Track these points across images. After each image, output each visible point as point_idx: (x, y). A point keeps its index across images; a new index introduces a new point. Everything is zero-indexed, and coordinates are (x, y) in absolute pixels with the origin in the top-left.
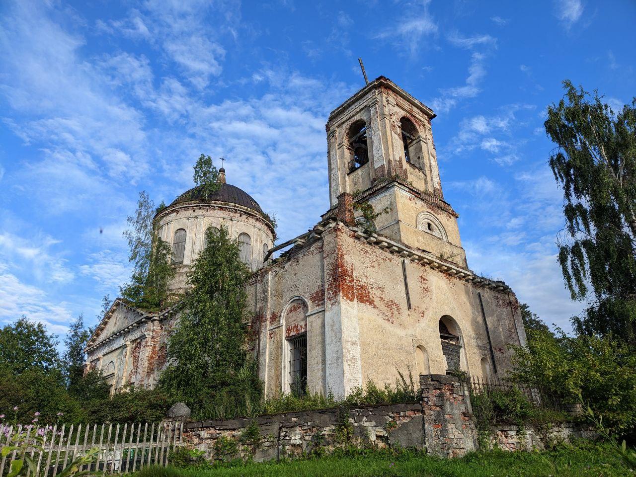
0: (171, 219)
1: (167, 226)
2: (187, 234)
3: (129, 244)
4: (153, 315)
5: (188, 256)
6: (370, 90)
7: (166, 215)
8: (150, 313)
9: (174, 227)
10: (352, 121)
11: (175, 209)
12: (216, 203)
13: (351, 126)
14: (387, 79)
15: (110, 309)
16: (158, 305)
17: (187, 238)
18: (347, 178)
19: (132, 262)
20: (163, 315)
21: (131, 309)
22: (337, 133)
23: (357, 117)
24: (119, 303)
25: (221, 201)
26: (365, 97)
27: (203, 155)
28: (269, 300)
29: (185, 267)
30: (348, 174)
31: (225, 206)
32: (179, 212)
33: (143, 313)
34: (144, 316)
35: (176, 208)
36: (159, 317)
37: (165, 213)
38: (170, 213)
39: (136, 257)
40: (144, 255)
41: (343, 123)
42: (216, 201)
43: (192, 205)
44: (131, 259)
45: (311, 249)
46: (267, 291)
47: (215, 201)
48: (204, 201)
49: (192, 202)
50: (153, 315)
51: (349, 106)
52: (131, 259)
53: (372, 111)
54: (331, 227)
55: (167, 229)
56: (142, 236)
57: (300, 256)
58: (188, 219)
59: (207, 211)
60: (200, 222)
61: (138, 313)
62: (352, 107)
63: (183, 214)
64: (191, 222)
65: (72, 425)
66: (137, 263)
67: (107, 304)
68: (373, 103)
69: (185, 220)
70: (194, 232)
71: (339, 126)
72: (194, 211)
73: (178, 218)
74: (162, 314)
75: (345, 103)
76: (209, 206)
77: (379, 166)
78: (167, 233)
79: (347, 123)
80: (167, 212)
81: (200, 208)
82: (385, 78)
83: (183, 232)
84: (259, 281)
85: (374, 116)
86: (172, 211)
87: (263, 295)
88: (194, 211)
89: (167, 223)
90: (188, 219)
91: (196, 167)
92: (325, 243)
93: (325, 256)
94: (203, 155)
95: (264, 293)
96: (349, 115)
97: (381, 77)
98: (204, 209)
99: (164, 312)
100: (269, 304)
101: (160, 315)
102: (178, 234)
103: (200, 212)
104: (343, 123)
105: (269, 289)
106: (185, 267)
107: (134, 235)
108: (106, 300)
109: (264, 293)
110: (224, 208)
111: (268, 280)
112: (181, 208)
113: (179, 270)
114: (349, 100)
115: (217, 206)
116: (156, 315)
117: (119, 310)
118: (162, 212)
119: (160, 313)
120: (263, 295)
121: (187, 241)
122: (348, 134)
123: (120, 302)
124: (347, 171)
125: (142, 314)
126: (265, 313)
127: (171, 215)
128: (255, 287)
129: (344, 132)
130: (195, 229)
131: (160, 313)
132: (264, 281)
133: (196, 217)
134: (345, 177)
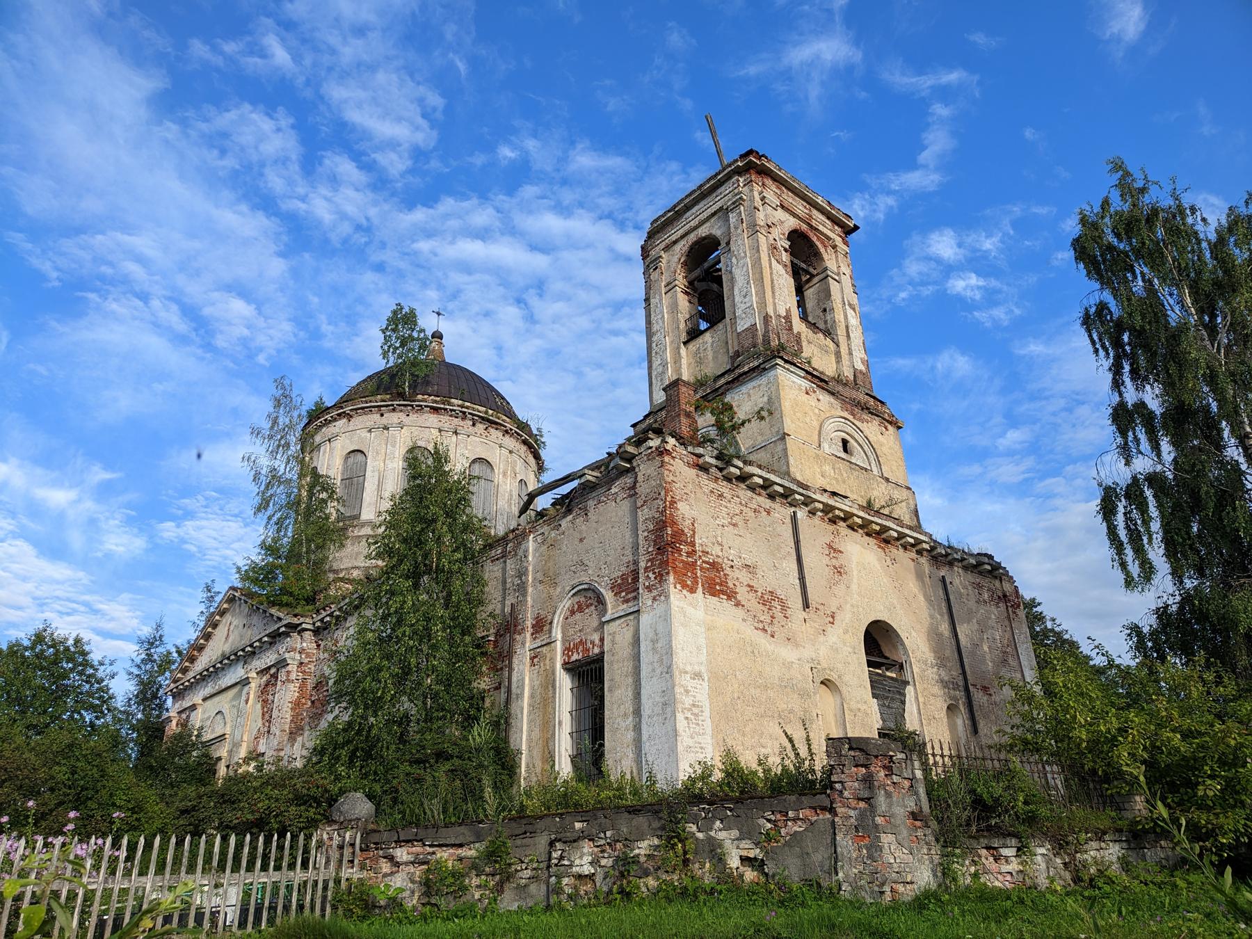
3: (254, 480)
6: (728, 177)
7: (327, 423)
8: (295, 616)
9: (342, 447)
10: (692, 237)
12: (424, 400)
13: (692, 248)
14: (763, 156)
16: (311, 600)
17: (369, 468)
18: (683, 351)
19: (260, 515)
20: (322, 620)
21: (258, 608)
22: (664, 261)
23: (703, 231)
26: (719, 191)
28: (530, 590)
30: (685, 343)
33: (281, 615)
34: (284, 622)
35: (347, 409)
36: (314, 624)
37: (326, 420)
38: (335, 420)
39: (268, 505)
41: (675, 242)
45: (613, 490)
46: (525, 573)
48: (401, 396)
50: (302, 620)
51: (688, 208)
53: (733, 217)
54: (651, 448)
56: (280, 465)
57: (591, 503)
58: (370, 431)
61: (272, 615)
62: (694, 210)
63: (360, 421)
66: (269, 518)
67: (211, 599)
68: (733, 203)
69: (365, 434)
71: (667, 249)
72: (382, 415)
73: (350, 429)
74: (319, 618)
75: (678, 203)
77: (746, 327)
79: (682, 243)
80: (328, 417)
81: (394, 410)
82: (757, 153)
83: (359, 457)
85: (736, 228)
86: (339, 415)
87: (517, 581)
88: (382, 415)
90: (370, 431)
91: (387, 328)
92: (640, 478)
93: (639, 504)
95: (520, 577)
96: (687, 227)
97: (750, 152)
99: (324, 614)
100: (529, 599)
101: (315, 620)
102: (351, 460)
103: (392, 418)
104: (675, 242)
105: (530, 568)
107: (265, 462)
109: (520, 577)
110: (441, 409)
111: (526, 551)
114: (687, 197)
115: (426, 406)
116: (308, 620)
117: (234, 610)
120: (517, 581)
122: (685, 264)
124: (684, 337)
125: (280, 619)
127: (337, 423)
129: (676, 260)
132: (520, 553)
134: (678, 348)
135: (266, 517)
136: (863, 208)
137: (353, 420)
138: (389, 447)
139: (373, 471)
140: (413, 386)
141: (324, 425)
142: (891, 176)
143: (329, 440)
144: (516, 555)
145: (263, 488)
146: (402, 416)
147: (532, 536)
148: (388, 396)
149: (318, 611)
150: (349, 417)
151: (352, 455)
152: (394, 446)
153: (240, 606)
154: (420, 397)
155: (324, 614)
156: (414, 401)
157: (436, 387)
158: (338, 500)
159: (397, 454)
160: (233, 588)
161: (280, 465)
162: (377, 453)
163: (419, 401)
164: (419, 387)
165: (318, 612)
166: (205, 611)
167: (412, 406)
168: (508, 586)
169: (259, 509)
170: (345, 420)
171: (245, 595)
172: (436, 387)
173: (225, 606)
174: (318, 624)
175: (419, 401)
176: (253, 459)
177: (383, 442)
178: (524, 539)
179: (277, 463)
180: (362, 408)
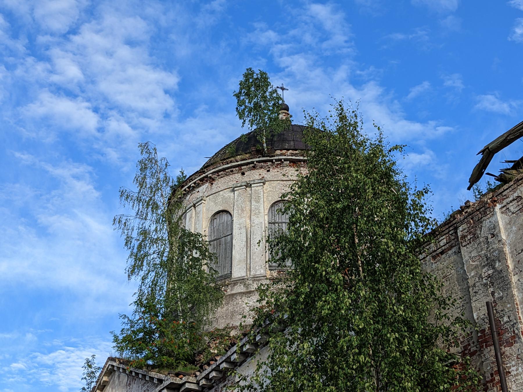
0: (201, 194)
1: (194, 210)
2: (234, 219)
3: (126, 244)
4: (185, 379)
5: (240, 261)
7: (191, 189)
8: (177, 375)
9: (208, 210)
11: (207, 177)
12: (282, 155)
15: (97, 382)
16: (191, 360)
17: (236, 226)
19: (133, 277)
20: (206, 377)
21: (137, 374)
24: (113, 366)
25: (292, 150)
27: (250, 69)
28: (514, 279)
29: (235, 283)
31: (302, 158)
32: (214, 180)
33: (162, 376)
34: (166, 383)
35: (209, 173)
36: (198, 383)
37: (189, 188)
38: (198, 185)
39: (142, 265)
40: (158, 261)
42: (284, 151)
43: (239, 163)
44: (132, 272)
46: (501, 256)
47: (281, 150)
48: (260, 152)
49: (238, 157)
50: (185, 379)
52: (132, 272)
55: (194, 215)
56: (150, 225)
58: (233, 191)
59: (268, 171)
60: (257, 192)
61: (152, 378)
63: (221, 183)
64: (238, 196)
65: (396, 374)
66: (144, 279)
67: (91, 375)
69: (228, 194)
70: (246, 214)
72: (243, 174)
73: (214, 191)
74: (204, 374)
76: (271, 161)
78: (195, 224)
80: (191, 184)
81: (254, 168)
83: (225, 217)
84: (464, 237)
86: (202, 180)
87: (487, 272)
88: (243, 174)
89: (194, 206)
90: (233, 191)
91: (240, 93)
94: (250, 69)
95: (490, 263)
98: (261, 168)
99: (209, 369)
100: (515, 292)
101: (199, 378)
102: (216, 222)
103: (254, 175)
105: (507, 250)
106: (235, 283)
107: (135, 223)
108: (90, 366)
109: (490, 263)
110: (300, 161)
111: (495, 226)
112: (218, 172)
113: (226, 291)
115: (286, 160)
116: (192, 379)
117: (114, 382)
118: (183, 187)
119: (198, 373)
120: (487, 272)
121: (235, 232)
123: (114, 364)
125: (160, 381)
126: (506, 319)
127: (200, 189)
128: (453, 258)
130: (248, 208)
131: (198, 373)
132: (484, 232)
133: (248, 185)
135: (140, 278)
136: (266, 311)
137: (215, 183)
138: (253, 203)
139: (240, 229)
140: (270, 142)
141: (188, 193)
142: (483, 96)
143: (194, 206)
144: (475, 237)
145: (135, 250)
146: (263, 172)
147: (498, 206)
148: (247, 156)
149: (201, 367)
150: (211, 180)
151: (217, 216)
152: (258, 202)
153: (119, 377)
154: (278, 152)
155: (209, 369)
156: (272, 156)
157: (292, 143)
158: (210, 257)
159: (262, 209)
160: (111, 359)
161: (150, 225)
162: (242, 210)
163: (277, 155)
164: (276, 144)
165: (201, 369)
166: (86, 387)
167: (271, 161)
168: (471, 282)
169: (132, 272)
170: (207, 184)
171: (123, 363)
172: (292, 143)
173: (105, 379)
174: (203, 382)
175: (277, 155)
176: (123, 221)
177: (247, 199)
178: (485, 214)
179: (147, 224)
180: (224, 170)
